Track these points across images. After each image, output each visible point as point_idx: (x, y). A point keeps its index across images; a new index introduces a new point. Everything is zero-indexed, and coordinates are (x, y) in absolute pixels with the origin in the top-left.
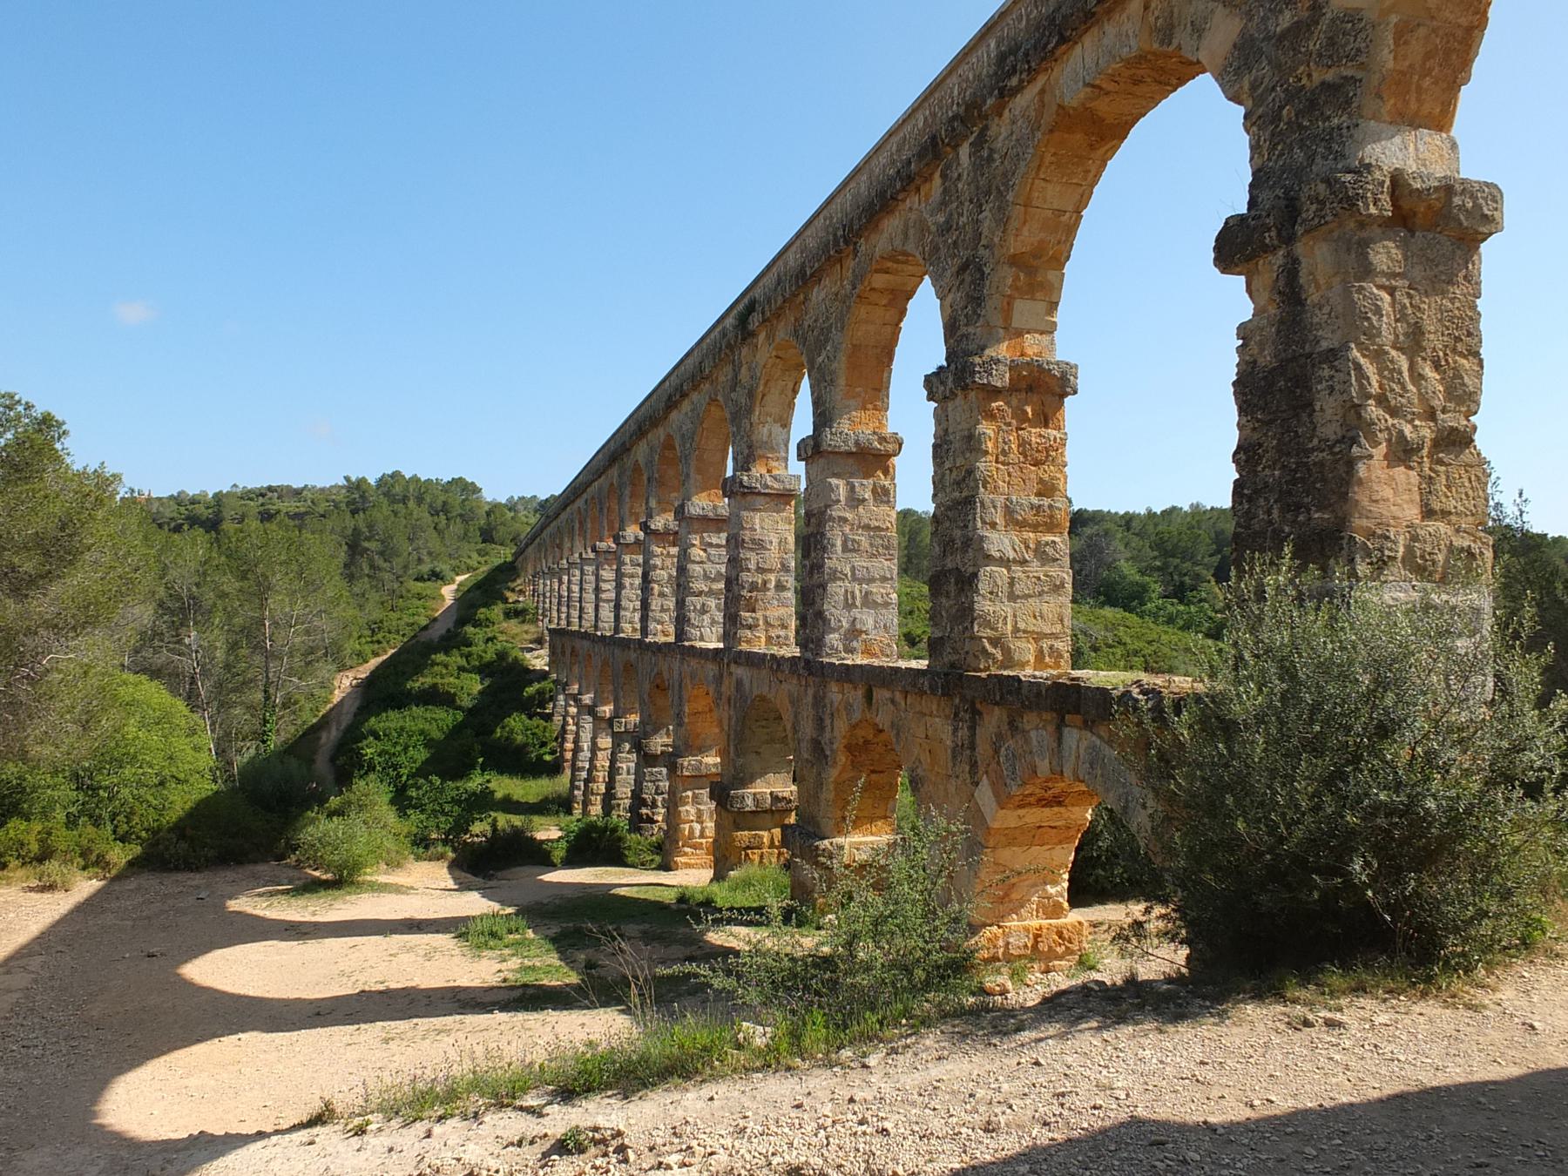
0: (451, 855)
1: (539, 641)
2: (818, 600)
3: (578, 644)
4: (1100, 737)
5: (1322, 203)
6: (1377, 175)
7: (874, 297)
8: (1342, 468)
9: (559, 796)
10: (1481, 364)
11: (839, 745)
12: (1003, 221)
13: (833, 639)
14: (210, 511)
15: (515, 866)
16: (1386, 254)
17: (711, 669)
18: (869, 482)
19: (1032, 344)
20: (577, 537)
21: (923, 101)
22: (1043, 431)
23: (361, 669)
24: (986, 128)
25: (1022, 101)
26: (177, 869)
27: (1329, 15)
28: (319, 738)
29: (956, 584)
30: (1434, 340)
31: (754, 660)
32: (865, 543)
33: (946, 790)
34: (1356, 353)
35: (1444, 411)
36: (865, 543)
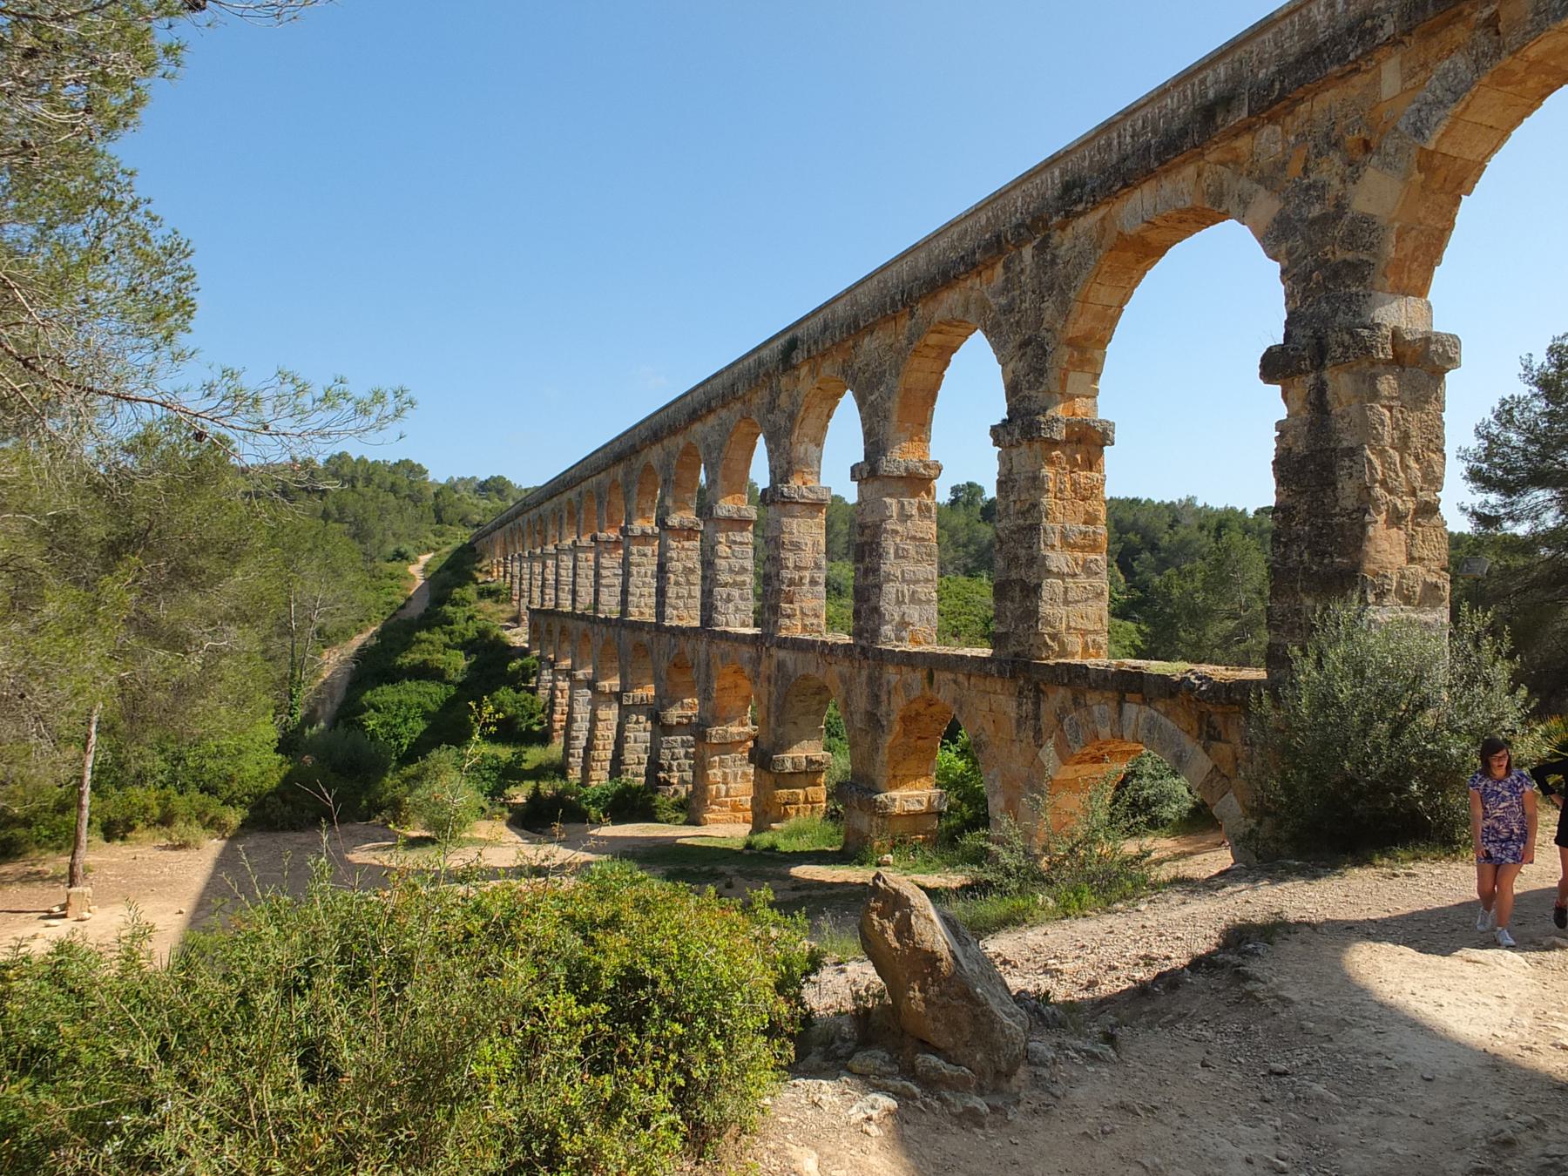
0: (507, 814)
1: (516, 620)
2: (873, 598)
3: (570, 624)
4: (1156, 710)
5: (1347, 348)
6: (1384, 331)
7: (926, 351)
8: (1357, 529)
9: (552, 763)
10: (1444, 457)
11: (895, 716)
12: (1064, 311)
13: (887, 630)
16: (1387, 384)
17: (747, 652)
18: (915, 501)
19: (1080, 405)
20: (565, 526)
21: (989, 203)
22: (1089, 474)
24: (1048, 236)
25: (1083, 223)
26: (283, 829)
27: (1350, 215)
29: (1021, 591)
30: (1416, 442)
31: (783, 643)
32: (912, 552)
33: (1010, 751)
34: (1368, 452)
35: (1421, 490)
36: (912, 552)
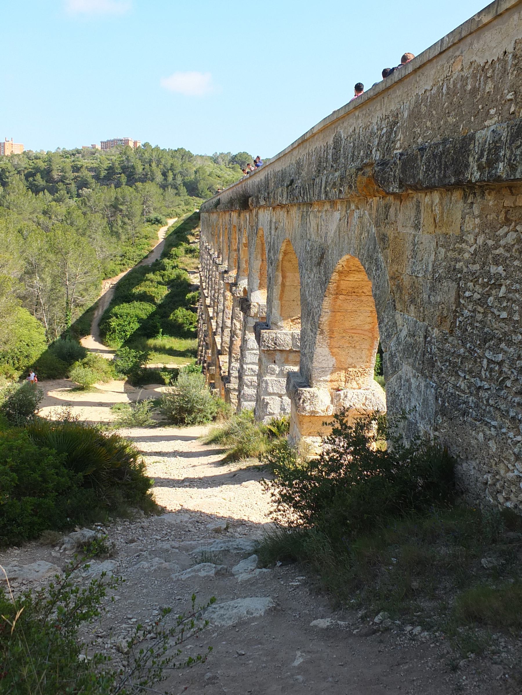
0: (127, 379)
9: (194, 349)
14: (46, 164)
15: (151, 384)
23: (114, 279)
28: (94, 314)
